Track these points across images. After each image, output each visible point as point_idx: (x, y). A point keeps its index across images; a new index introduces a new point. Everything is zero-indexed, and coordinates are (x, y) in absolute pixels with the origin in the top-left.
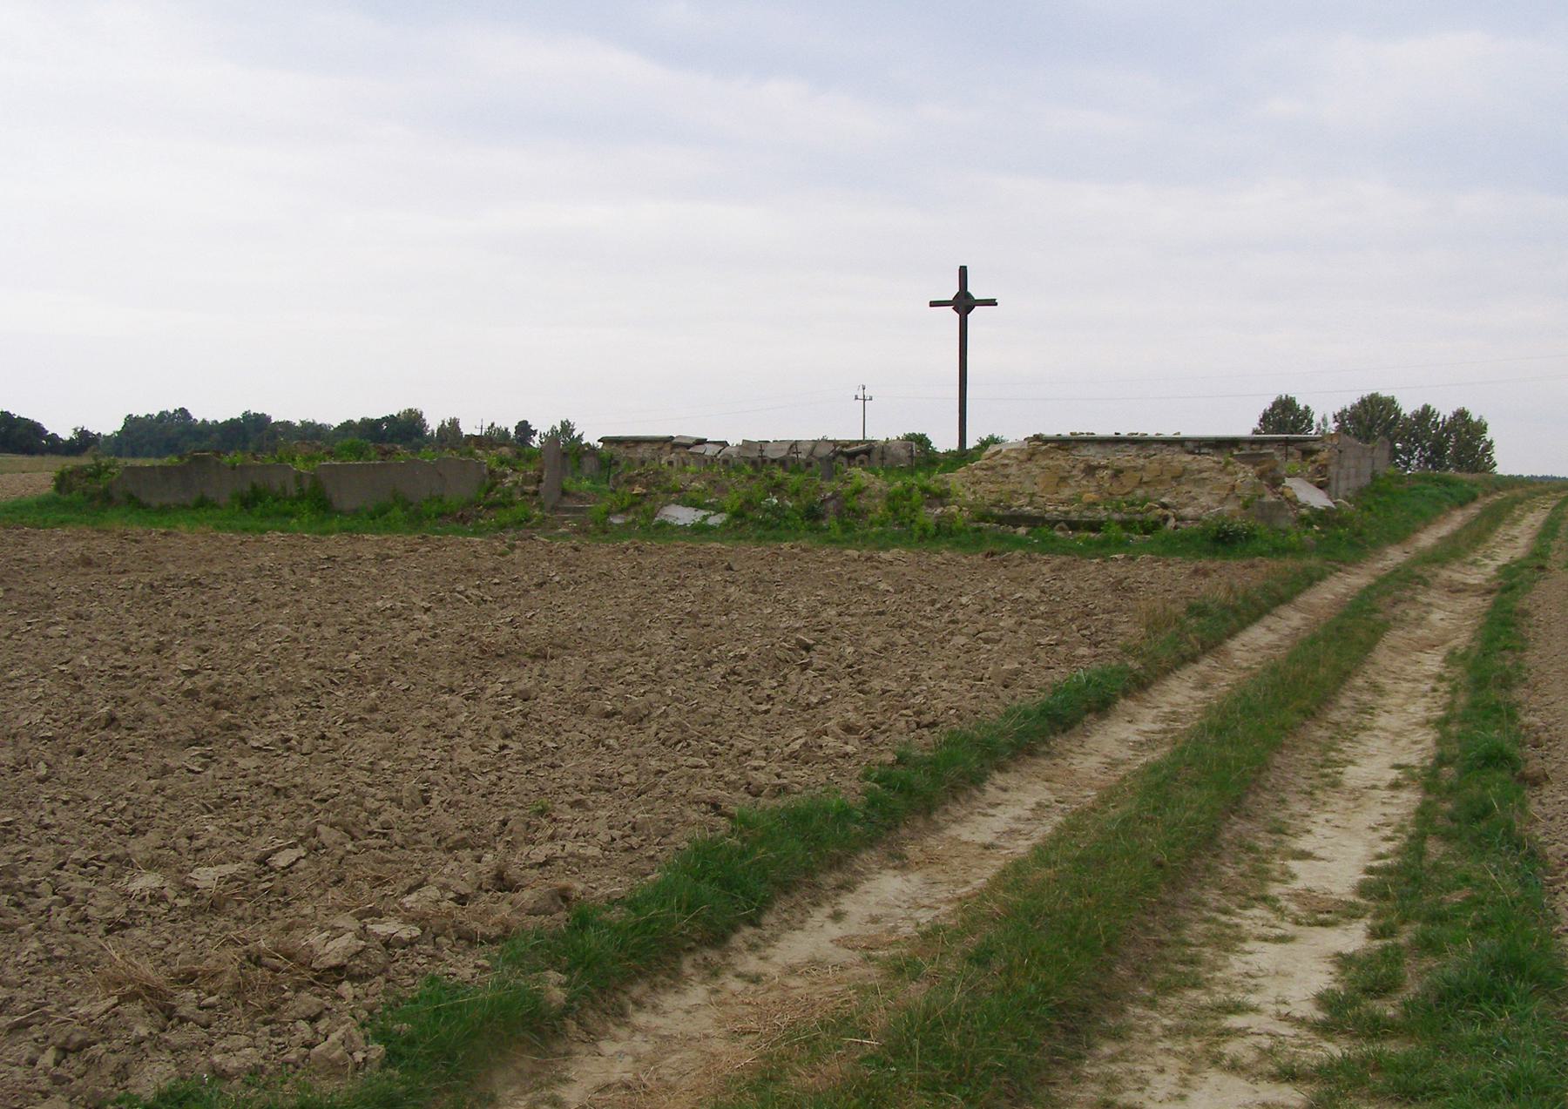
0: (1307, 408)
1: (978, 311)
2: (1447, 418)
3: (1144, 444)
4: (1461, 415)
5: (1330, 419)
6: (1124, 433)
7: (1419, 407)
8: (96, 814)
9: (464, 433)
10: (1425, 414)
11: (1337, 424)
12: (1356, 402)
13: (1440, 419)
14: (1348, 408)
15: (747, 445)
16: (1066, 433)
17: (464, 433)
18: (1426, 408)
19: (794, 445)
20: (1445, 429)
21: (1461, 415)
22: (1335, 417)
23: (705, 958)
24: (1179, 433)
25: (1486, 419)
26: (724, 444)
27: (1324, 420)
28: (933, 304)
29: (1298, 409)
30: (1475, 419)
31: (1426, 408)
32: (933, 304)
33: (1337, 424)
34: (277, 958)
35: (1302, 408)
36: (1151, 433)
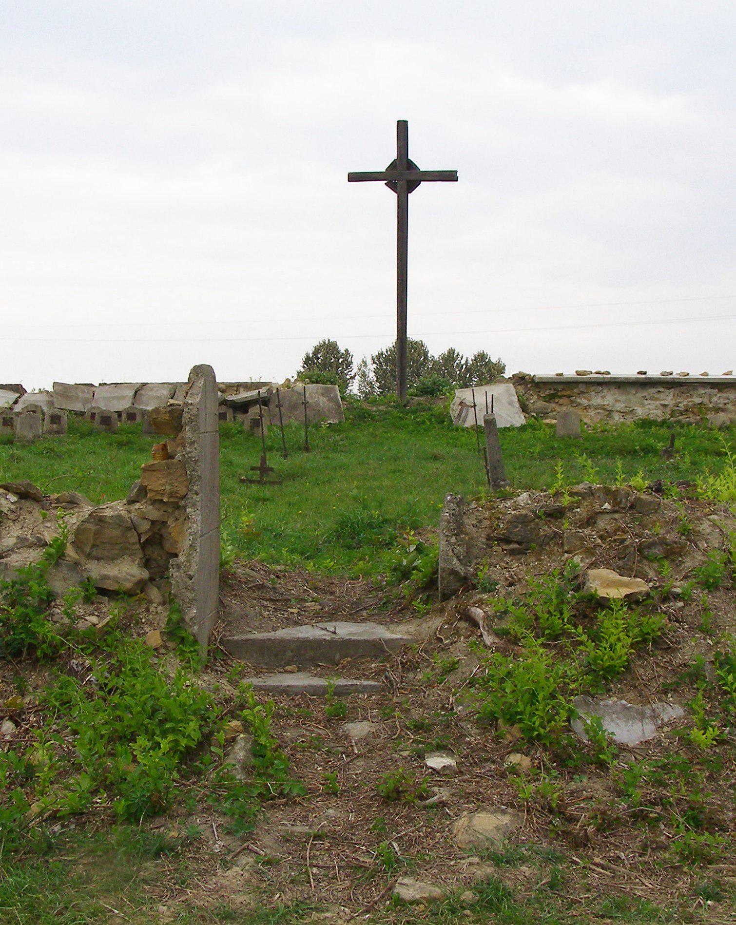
0: (347, 351)
1: (392, 197)
2: (469, 359)
3: (683, 389)
4: (482, 357)
5: (369, 361)
6: (654, 372)
7: (445, 350)
8: (310, 853)
9: (498, 427)
10: (451, 357)
11: (375, 366)
12: (391, 346)
13: (463, 362)
14: (384, 351)
15: (62, 390)
16: (569, 372)
17: (498, 427)
18: (451, 352)
19: (140, 390)
20: (468, 370)
21: (482, 357)
22: (373, 359)
23: (653, 710)
24: (730, 373)
25: (504, 361)
26: (18, 389)
27: (365, 363)
28: (354, 177)
29: (338, 352)
30: (494, 360)
31: (451, 352)
32: (354, 177)
33: (375, 366)
34: (318, 728)
35: (342, 351)
36: (695, 373)
